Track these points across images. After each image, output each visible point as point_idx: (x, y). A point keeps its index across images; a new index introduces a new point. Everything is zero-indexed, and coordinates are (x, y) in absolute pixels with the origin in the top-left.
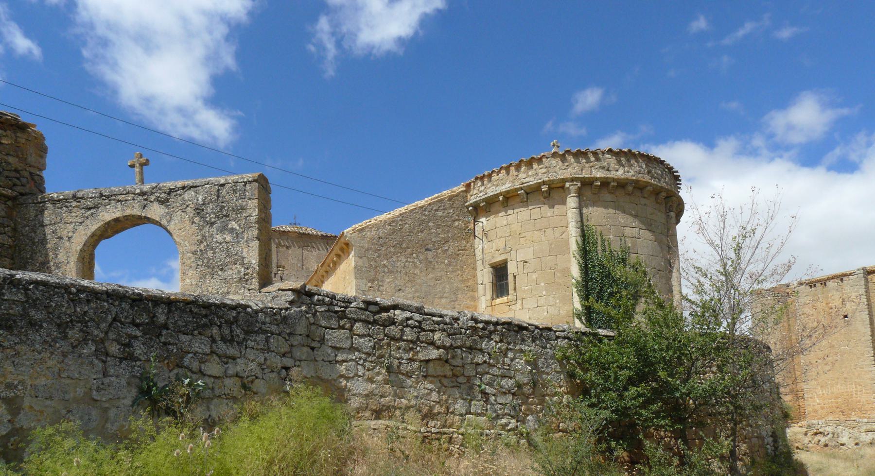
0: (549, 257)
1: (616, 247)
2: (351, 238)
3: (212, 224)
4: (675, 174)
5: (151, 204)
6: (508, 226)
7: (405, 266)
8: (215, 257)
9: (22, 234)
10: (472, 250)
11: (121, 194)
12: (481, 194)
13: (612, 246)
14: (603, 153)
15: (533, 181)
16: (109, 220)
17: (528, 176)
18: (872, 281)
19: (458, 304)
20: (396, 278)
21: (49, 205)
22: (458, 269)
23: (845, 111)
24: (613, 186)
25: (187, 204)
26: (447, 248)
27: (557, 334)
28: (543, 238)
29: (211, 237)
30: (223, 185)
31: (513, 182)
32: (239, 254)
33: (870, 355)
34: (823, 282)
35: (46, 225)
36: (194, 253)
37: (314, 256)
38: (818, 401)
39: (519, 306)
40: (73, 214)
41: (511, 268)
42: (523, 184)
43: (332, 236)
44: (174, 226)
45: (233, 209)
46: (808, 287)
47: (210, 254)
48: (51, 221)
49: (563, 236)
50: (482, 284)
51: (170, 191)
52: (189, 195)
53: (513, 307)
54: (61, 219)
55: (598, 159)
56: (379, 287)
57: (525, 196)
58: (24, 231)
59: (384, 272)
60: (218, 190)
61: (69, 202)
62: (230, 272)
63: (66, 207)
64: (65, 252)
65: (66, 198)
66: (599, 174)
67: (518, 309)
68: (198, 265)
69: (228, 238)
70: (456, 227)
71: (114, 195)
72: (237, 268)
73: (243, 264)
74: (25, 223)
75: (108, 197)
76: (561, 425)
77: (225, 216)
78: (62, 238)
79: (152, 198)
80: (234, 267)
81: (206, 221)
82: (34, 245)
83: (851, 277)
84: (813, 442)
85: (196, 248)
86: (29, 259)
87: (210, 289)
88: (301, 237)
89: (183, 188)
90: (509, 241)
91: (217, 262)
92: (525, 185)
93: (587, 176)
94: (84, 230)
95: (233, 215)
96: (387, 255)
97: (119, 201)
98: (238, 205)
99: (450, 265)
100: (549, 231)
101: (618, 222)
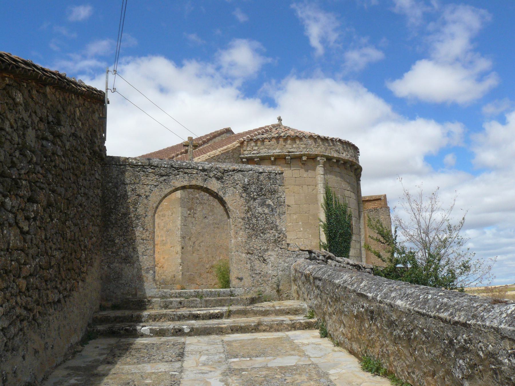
0: (305, 205)
1: (341, 202)
3: (255, 199)
5: (210, 179)
7: (208, 199)
8: (258, 223)
9: (107, 188)
11: (188, 168)
12: (254, 152)
13: (340, 202)
21: (129, 168)
23: (270, 60)
25: (237, 183)
29: (254, 208)
30: (261, 173)
31: (281, 149)
32: (274, 223)
35: (127, 184)
36: (243, 219)
45: (269, 190)
47: (254, 221)
48: (131, 181)
49: (314, 192)
51: (225, 171)
52: (238, 176)
54: (139, 181)
55: (334, 145)
58: (108, 186)
59: (197, 203)
60: (259, 176)
61: (145, 168)
62: (268, 235)
63: (143, 171)
64: (143, 207)
65: (144, 164)
66: (336, 155)
68: (246, 228)
69: (266, 211)
71: (182, 168)
72: (273, 232)
73: (277, 230)
74: (109, 179)
75: (177, 169)
77: (263, 195)
78: (141, 196)
79: (212, 175)
80: (271, 231)
81: (251, 197)
82: (116, 199)
85: (244, 216)
86: (113, 209)
87: (255, 246)
89: (234, 170)
91: (259, 227)
94: (159, 192)
95: (269, 195)
97: (185, 173)
98: (272, 188)
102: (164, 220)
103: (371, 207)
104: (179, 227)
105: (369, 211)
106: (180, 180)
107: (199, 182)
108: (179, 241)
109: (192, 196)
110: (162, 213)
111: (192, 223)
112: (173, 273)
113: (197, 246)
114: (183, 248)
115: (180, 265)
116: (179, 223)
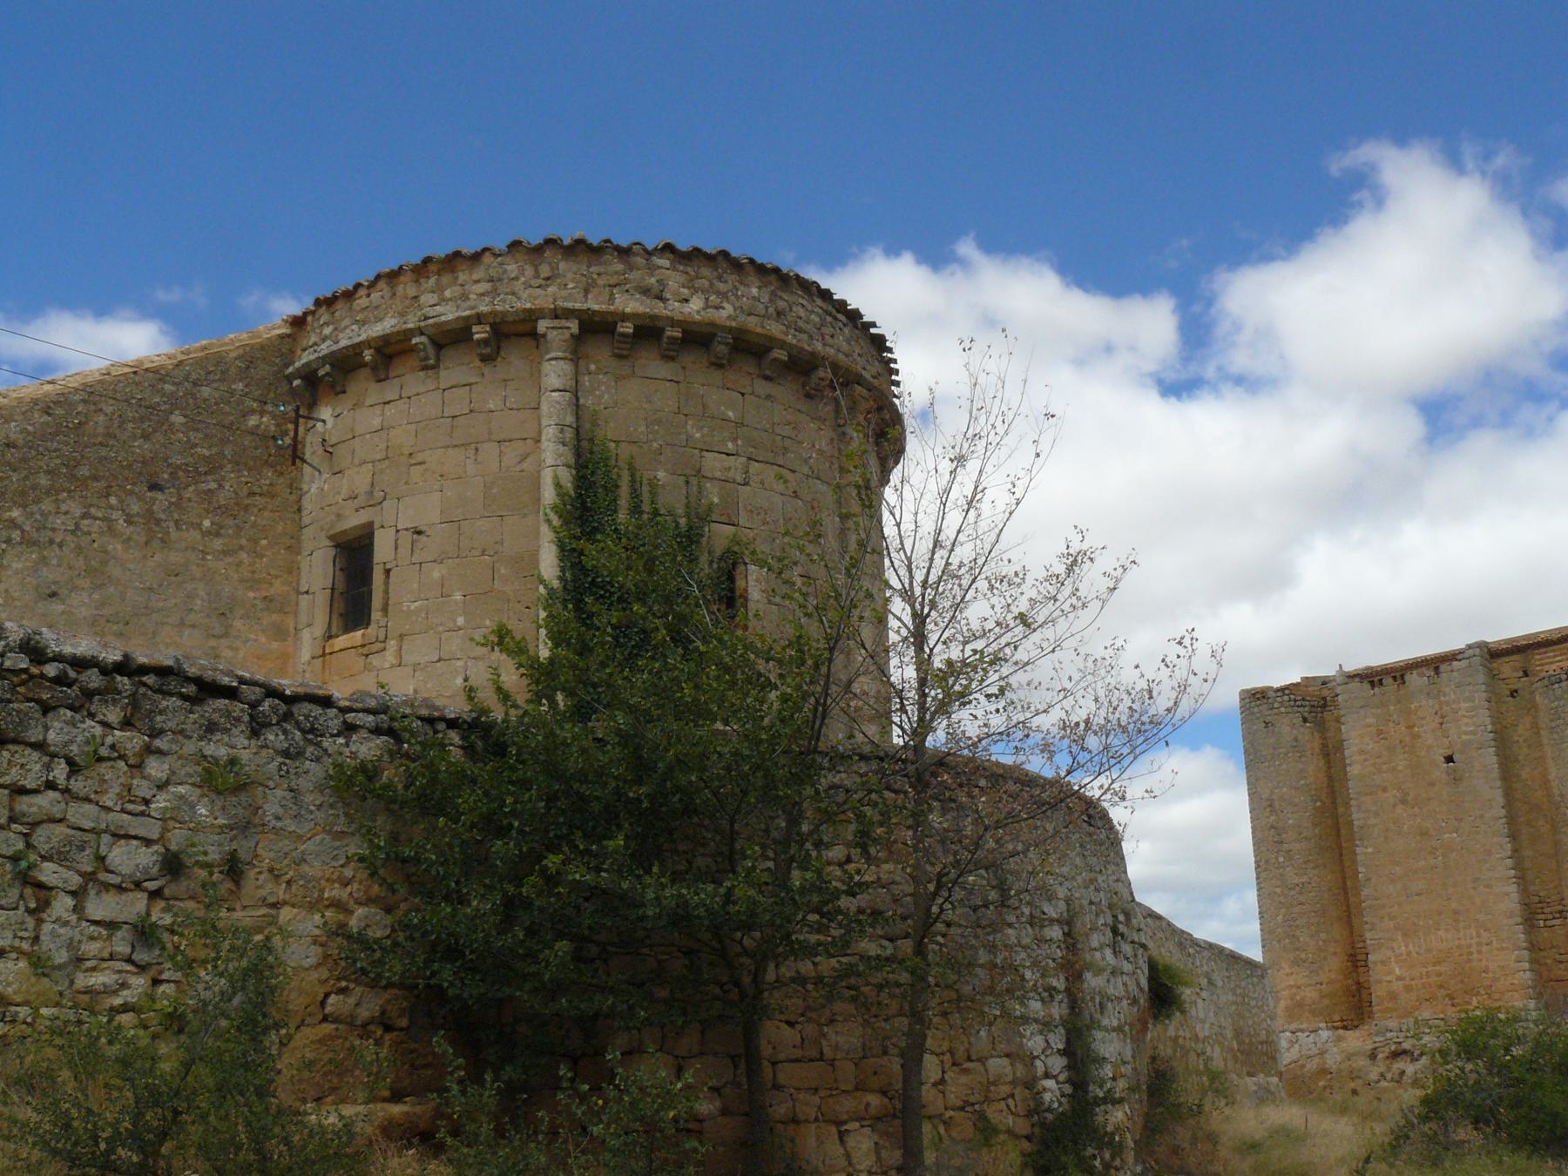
1: (673, 499)
4: (873, 331)
6: (383, 434)
10: (293, 498)
14: (649, 254)
15: (449, 314)
17: (442, 300)
18: (1501, 676)
19: (230, 648)
20: (43, 560)
22: (241, 548)
24: (672, 339)
26: (213, 485)
27: (350, 717)
28: (471, 468)
31: (402, 314)
33: (1503, 854)
34: (1398, 675)
38: (1398, 971)
39: (390, 657)
41: (383, 549)
42: (426, 318)
46: (1366, 686)
49: (525, 465)
50: (307, 592)
53: (375, 660)
57: (431, 351)
66: (631, 304)
67: (387, 665)
70: (252, 432)
76: (332, 999)
83: (1455, 663)
84: (1389, 1076)
90: (382, 471)
92: (431, 321)
93: (596, 307)
96: (23, 493)
99: (218, 535)
100: (490, 450)
101: (684, 437)
103: (1554, 667)
105: (1546, 682)
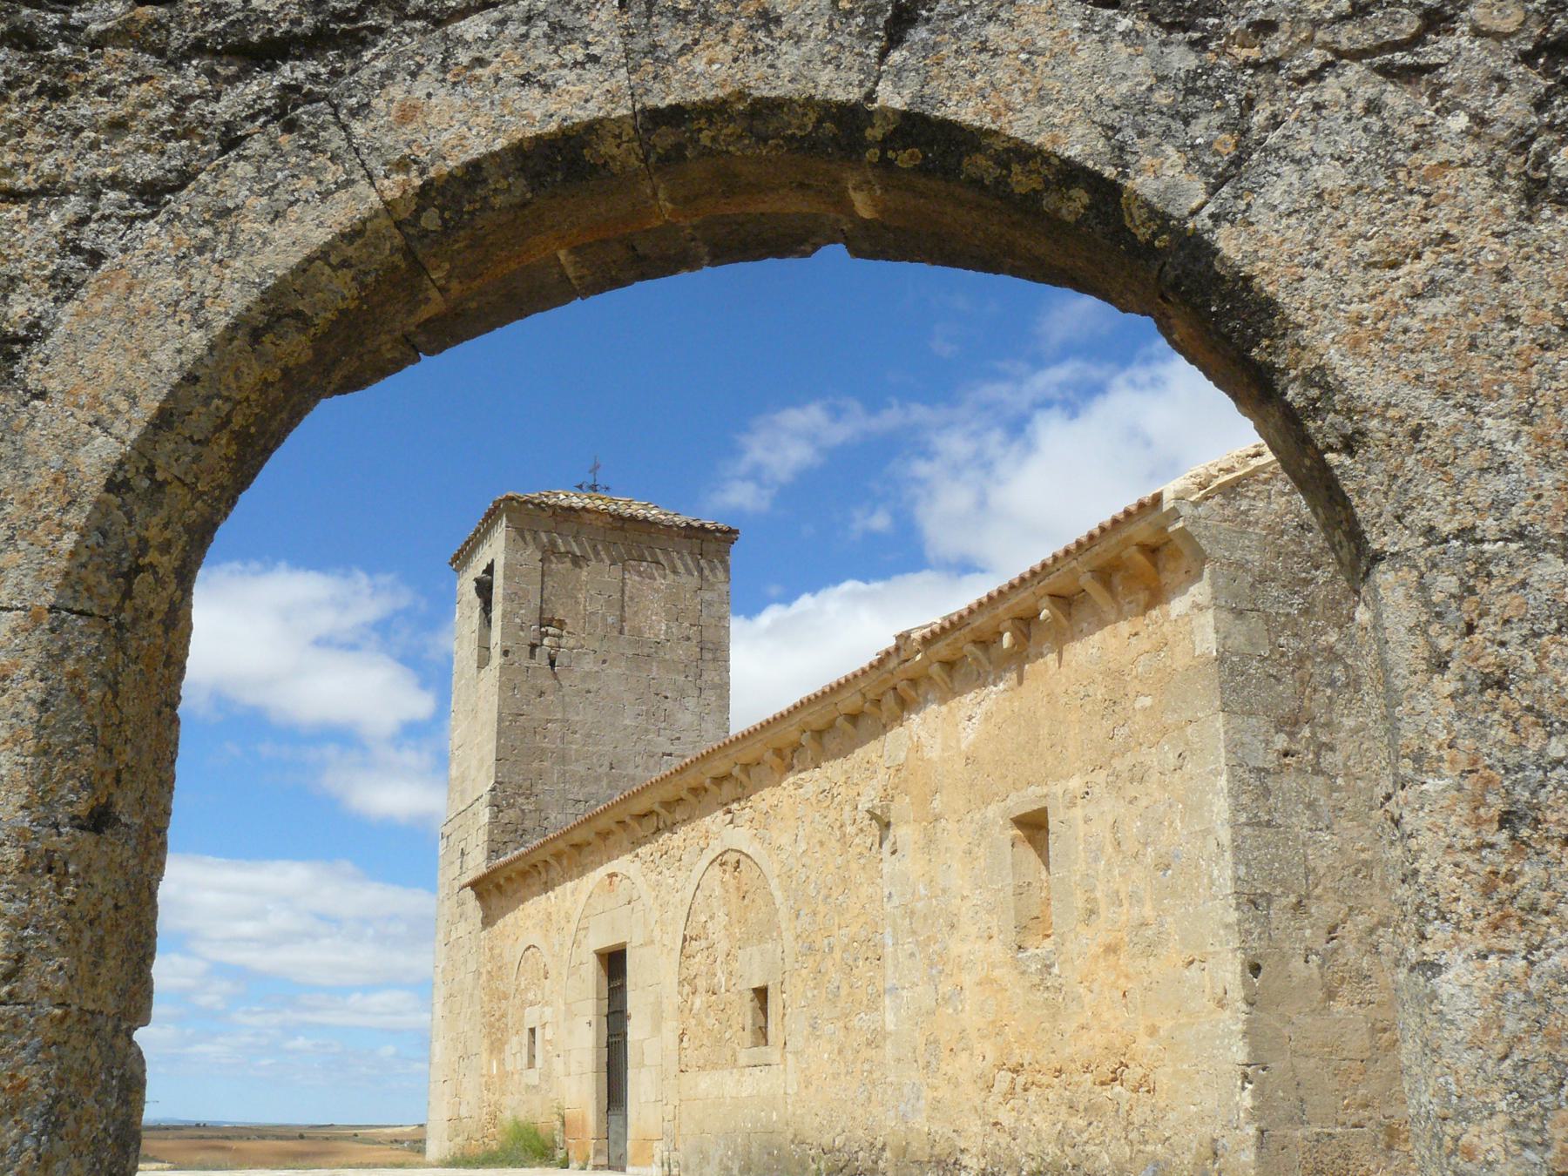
2: (1195, 520)
16: (477, 148)
37: (657, 591)
40: (84, 108)
43: (718, 530)
44: (1299, 233)
56: (1317, 755)
59: (1332, 683)
88: (622, 529)
102: (1144, 802)
104: (1225, 835)
106: (506, 62)
107: (791, 56)
108: (1227, 926)
109: (1293, 643)
110: (1130, 759)
111: (1310, 805)
112: (1207, 1131)
113: (1351, 953)
114: (1255, 969)
115: (1245, 1077)
116: (1220, 807)
